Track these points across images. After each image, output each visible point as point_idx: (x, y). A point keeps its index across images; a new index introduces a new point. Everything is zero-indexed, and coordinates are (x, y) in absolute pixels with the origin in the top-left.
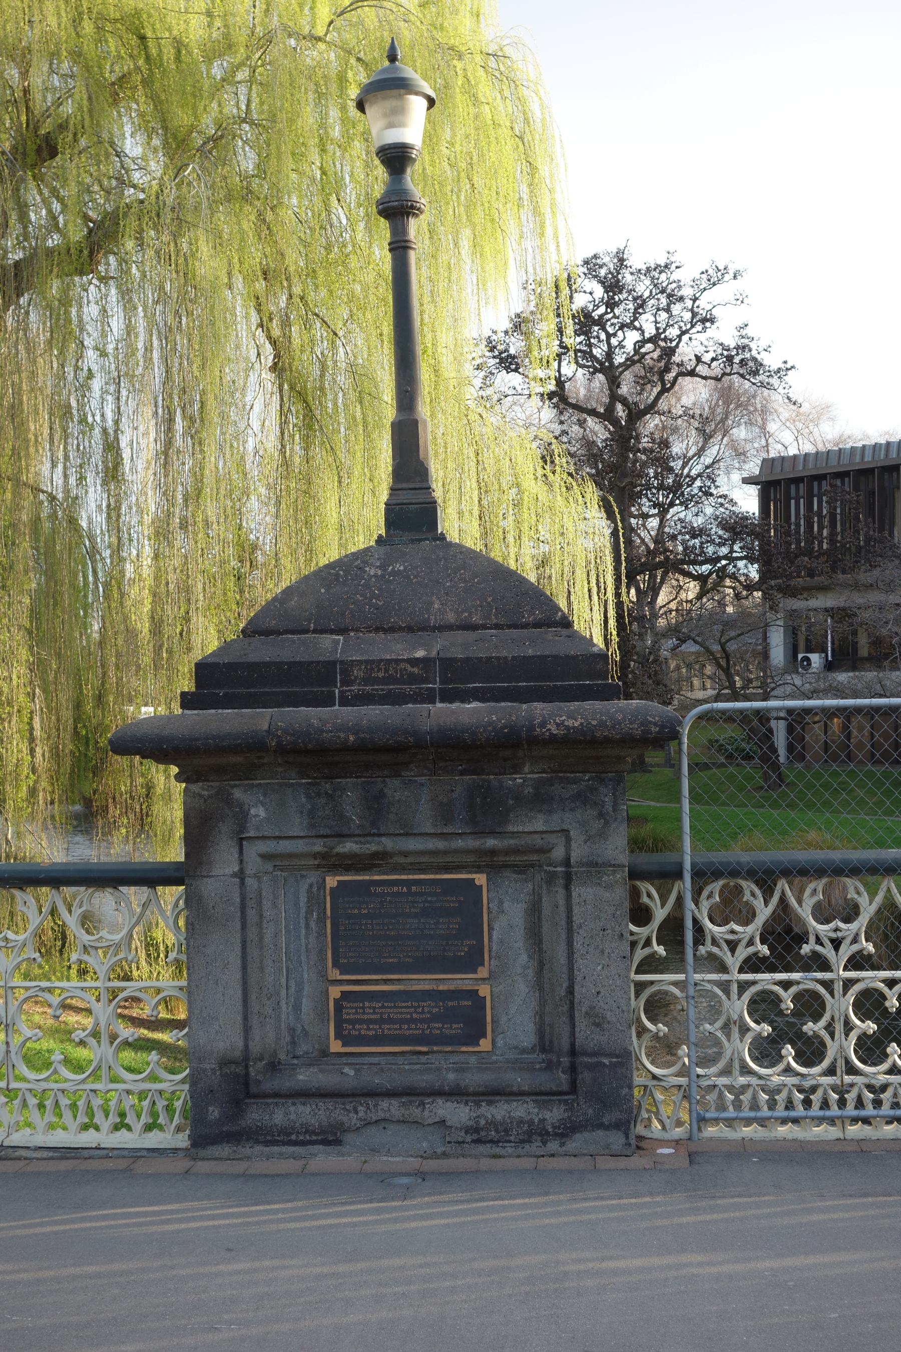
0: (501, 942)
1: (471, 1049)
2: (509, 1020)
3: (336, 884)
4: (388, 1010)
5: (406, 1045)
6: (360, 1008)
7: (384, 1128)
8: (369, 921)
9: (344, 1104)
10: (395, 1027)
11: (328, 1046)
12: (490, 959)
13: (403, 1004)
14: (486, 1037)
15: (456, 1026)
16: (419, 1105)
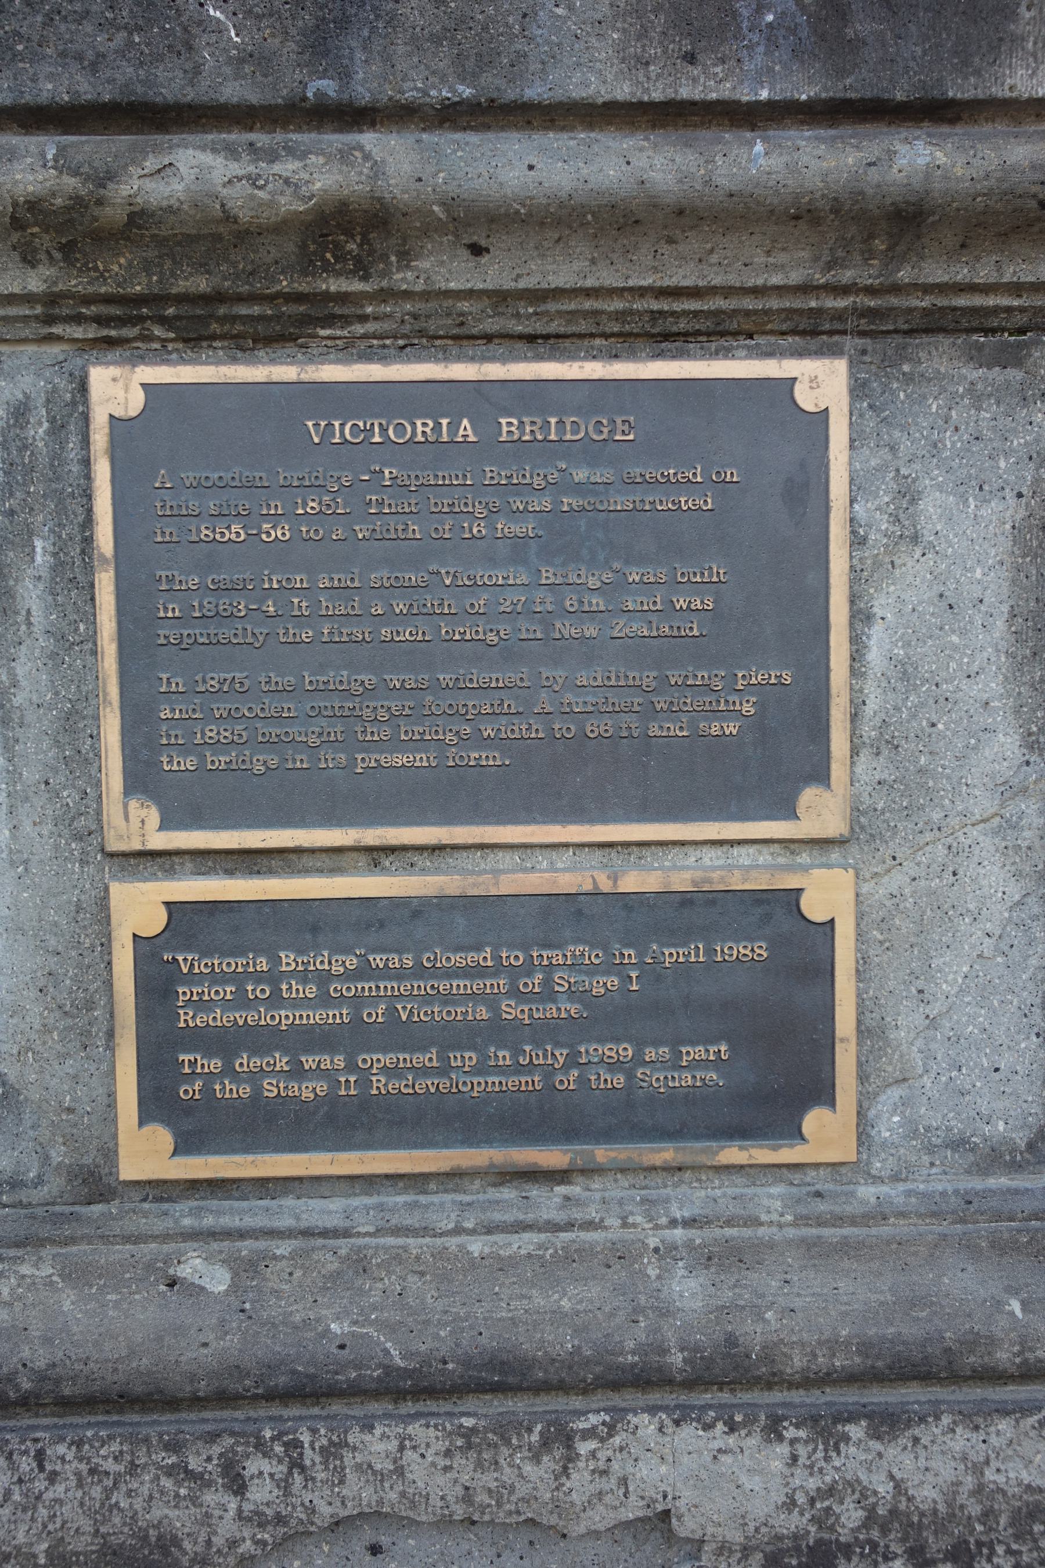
0: (905, 676)
1: (762, 1155)
2: (933, 1023)
3: (135, 402)
4: (388, 985)
5: (469, 1140)
6: (258, 977)
7: (375, 1550)
8: (299, 580)
9: (173, 1446)
10: (420, 1059)
11: (110, 1154)
12: (855, 752)
13: (458, 959)
14: (832, 1103)
15: (697, 1052)
16: (546, 1443)
